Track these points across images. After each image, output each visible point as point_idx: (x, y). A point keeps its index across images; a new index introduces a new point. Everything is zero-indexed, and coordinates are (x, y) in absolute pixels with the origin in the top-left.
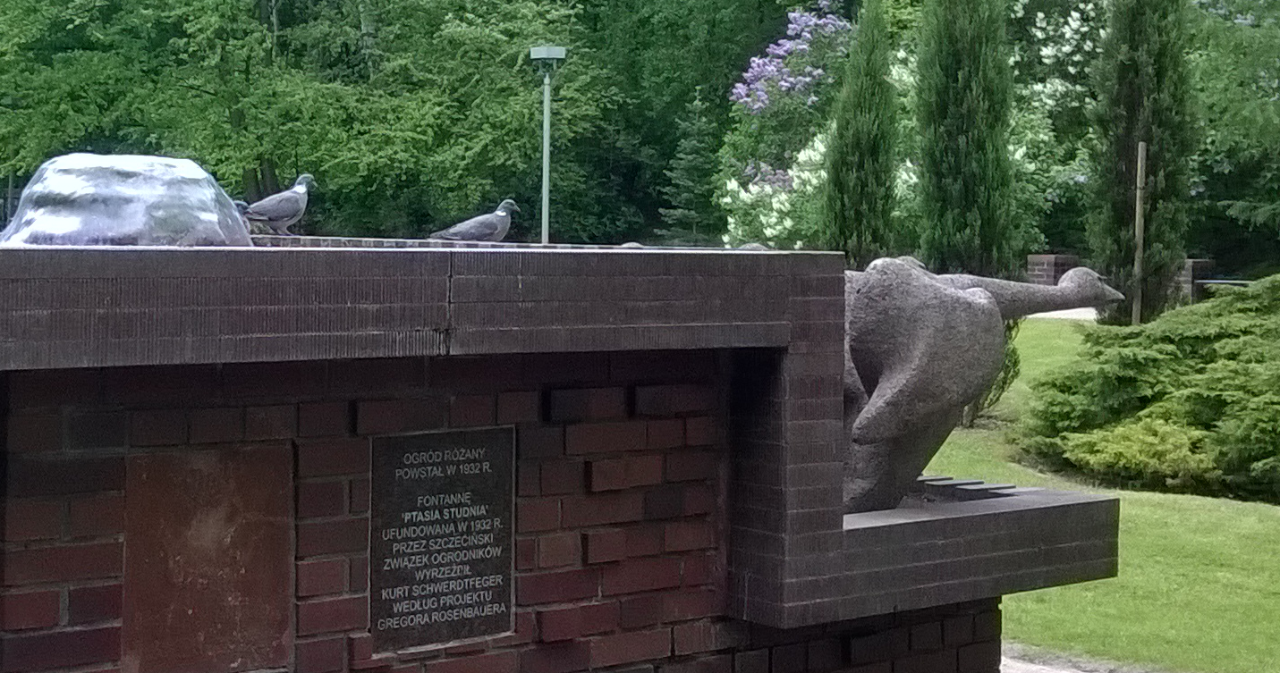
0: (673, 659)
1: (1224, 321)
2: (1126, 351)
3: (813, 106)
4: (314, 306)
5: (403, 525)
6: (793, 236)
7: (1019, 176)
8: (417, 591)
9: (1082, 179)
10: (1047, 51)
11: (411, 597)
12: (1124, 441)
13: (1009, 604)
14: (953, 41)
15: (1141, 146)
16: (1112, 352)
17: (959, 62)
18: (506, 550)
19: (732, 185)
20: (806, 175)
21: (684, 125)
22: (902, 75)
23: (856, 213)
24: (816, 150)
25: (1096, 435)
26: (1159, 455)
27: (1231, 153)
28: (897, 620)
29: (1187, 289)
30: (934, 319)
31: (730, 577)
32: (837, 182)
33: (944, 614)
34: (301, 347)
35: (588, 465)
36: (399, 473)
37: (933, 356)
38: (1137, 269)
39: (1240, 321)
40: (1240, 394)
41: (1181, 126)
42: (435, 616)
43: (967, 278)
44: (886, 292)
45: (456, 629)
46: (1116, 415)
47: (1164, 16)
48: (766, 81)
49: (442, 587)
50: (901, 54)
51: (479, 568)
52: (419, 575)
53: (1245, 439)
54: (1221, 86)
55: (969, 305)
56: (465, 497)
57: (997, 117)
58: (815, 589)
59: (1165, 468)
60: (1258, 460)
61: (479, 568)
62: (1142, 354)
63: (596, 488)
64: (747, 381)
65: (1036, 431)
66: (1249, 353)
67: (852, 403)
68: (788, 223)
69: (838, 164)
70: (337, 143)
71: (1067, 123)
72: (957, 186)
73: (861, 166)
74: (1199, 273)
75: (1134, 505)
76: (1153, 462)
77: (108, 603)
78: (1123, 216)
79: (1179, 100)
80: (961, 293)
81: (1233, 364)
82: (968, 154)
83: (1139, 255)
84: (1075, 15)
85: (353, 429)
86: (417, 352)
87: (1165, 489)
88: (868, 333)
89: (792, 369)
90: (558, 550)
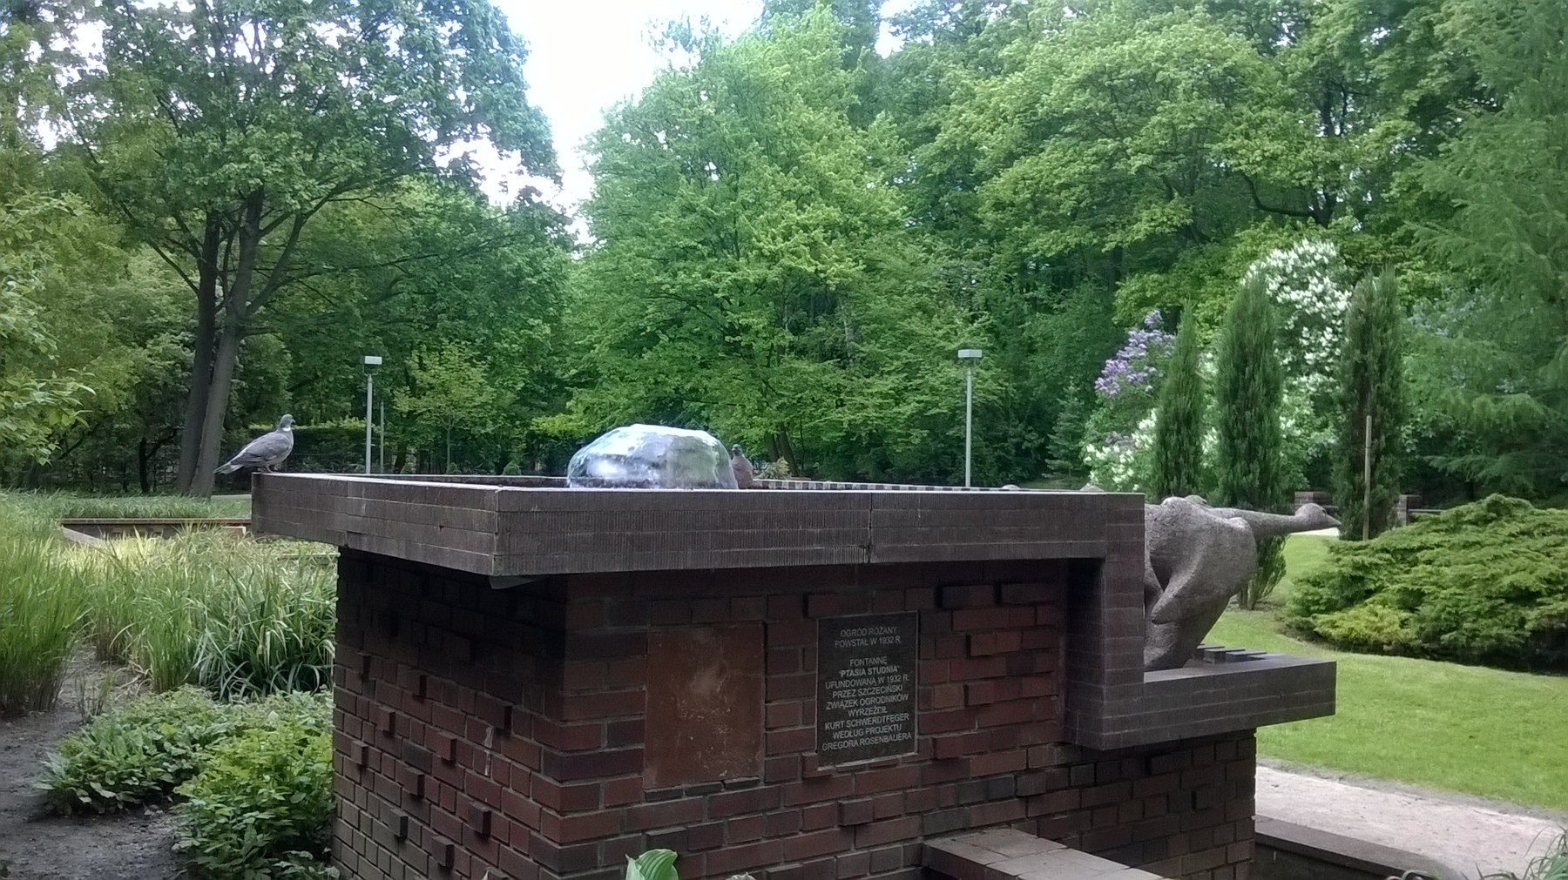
0: (1028, 771)
1: (1423, 538)
2: (1357, 559)
3: (1150, 392)
4: (776, 530)
5: (839, 679)
6: (1134, 480)
7: (1289, 439)
8: (849, 724)
9: (1332, 441)
10: (1309, 356)
11: (845, 728)
12: (1356, 620)
13: (1262, 732)
14: (1242, 347)
15: (1369, 419)
16: (1347, 559)
17: (1246, 361)
18: (911, 696)
19: (1091, 448)
20: (1144, 437)
21: (1063, 402)
22: (1209, 367)
23: (1175, 467)
24: (1150, 422)
25: (1336, 616)
26: (1379, 630)
27: (1434, 424)
28: (1181, 745)
29: (1401, 515)
30: (1206, 540)
31: (1067, 715)
32: (1163, 442)
33: (1217, 740)
34: (769, 557)
35: (968, 638)
36: (837, 643)
37: (1207, 563)
38: (1366, 502)
39: (1434, 538)
40: (1434, 588)
41: (1396, 406)
42: (863, 742)
43: (1232, 510)
44: (1175, 520)
45: (875, 750)
46: (1350, 602)
47: (1385, 330)
48: (1116, 377)
49: (867, 721)
50: (1209, 355)
51: (893, 708)
52: (851, 713)
53: (1437, 619)
54: (1425, 378)
55: (1231, 530)
56: (883, 661)
57: (1272, 398)
58: (1124, 723)
59: (1383, 638)
60: (1445, 632)
61: (893, 708)
62: (1367, 560)
63: (974, 652)
64: (1078, 581)
65: (1297, 613)
66: (1441, 560)
67: (1150, 596)
68: (1131, 472)
69: (1163, 432)
70: (829, 407)
71: (1322, 403)
72: (1244, 446)
73: (1179, 432)
74: (1411, 505)
75: (1349, 664)
76: (1374, 634)
77: (634, 732)
78: (1357, 466)
79: (1395, 387)
80: (1226, 521)
81: (1429, 568)
82: (1251, 424)
83: (1367, 492)
84: (1329, 330)
85: (805, 612)
86: (848, 561)
87: (1383, 653)
88: (1162, 548)
89: (1108, 573)
90: (948, 696)
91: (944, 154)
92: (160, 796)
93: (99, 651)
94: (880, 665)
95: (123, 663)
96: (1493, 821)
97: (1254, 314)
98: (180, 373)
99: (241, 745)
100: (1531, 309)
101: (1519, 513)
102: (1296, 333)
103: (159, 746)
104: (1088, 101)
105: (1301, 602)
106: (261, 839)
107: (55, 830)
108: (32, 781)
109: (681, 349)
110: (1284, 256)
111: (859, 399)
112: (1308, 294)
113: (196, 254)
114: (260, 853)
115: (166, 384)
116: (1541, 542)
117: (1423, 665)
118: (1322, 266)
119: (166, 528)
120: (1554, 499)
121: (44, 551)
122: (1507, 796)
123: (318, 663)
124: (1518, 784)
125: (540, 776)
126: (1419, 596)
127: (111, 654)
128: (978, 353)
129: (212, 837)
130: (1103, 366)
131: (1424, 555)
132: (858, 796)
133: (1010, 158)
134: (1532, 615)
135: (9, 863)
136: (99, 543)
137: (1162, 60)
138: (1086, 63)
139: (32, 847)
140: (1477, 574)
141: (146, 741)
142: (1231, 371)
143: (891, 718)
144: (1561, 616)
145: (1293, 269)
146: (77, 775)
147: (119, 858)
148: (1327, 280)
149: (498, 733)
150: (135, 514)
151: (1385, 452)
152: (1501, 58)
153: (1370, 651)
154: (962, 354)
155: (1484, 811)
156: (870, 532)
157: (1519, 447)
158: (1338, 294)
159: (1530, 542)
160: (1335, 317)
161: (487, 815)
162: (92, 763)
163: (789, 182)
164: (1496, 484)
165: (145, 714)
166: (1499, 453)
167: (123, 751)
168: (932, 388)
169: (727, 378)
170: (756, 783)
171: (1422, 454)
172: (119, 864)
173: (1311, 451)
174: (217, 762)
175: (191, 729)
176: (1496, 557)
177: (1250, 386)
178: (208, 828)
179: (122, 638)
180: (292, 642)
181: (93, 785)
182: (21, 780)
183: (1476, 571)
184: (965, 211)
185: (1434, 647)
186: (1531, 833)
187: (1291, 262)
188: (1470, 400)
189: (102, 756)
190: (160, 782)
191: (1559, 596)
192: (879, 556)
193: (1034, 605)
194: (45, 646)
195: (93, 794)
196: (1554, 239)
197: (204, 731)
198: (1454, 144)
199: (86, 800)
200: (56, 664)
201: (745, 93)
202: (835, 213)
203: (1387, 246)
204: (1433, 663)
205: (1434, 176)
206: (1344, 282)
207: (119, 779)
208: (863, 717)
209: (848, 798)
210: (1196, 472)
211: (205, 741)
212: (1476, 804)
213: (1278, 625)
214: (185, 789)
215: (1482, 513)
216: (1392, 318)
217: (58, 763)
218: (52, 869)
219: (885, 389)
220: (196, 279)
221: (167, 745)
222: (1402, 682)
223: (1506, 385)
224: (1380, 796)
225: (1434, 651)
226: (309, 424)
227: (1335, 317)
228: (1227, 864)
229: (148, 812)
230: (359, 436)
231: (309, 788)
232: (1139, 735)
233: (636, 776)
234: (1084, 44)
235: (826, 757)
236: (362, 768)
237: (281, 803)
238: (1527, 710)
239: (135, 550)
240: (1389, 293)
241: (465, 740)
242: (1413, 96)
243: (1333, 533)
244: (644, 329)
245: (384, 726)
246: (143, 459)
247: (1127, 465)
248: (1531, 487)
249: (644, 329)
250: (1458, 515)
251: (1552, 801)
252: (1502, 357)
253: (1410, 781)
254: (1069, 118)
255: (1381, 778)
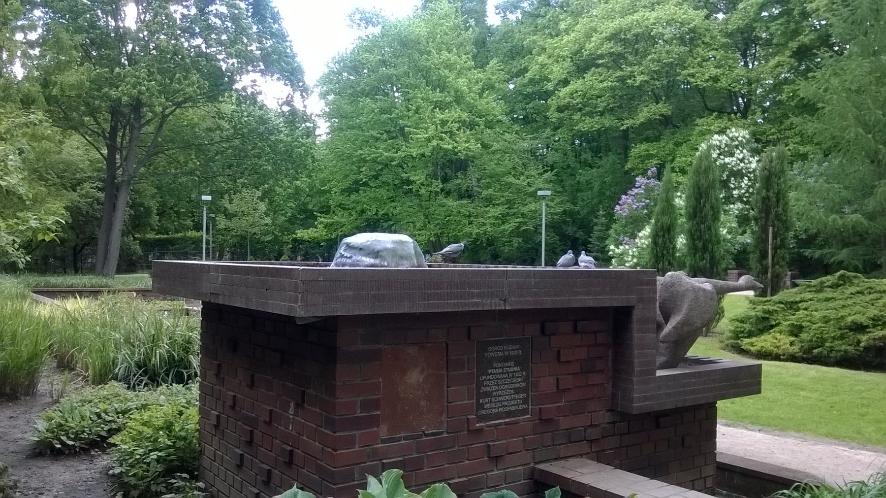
0: (591, 426)
1: (802, 296)
2: (765, 307)
3: (646, 214)
4: (454, 290)
5: (488, 375)
6: (636, 265)
7: (724, 240)
10: (735, 192)
12: (765, 342)
13: (720, 404)
14: (699, 188)
15: (771, 229)
17: (701, 196)
19: (612, 247)
20: (643, 241)
21: (595, 220)
22: (680, 201)
23: (662, 255)
24: (647, 231)
25: (754, 339)
26: (778, 347)
27: (806, 231)
28: (677, 411)
29: (789, 283)
30: (691, 295)
32: (655, 243)
33: (695, 408)
35: (559, 351)
37: (691, 309)
38: (769, 275)
39: (808, 296)
42: (501, 409)
44: (673, 285)
45: (509, 414)
46: (761, 332)
47: (779, 179)
48: (627, 205)
49: (502, 398)
50: (679, 194)
51: (517, 391)
52: (494, 394)
53: (811, 341)
55: (704, 290)
56: (512, 364)
57: (716, 218)
59: (780, 352)
61: (517, 391)
62: (771, 308)
63: (562, 359)
64: (618, 320)
65: (731, 338)
66: (813, 308)
67: (659, 327)
68: (635, 260)
69: (655, 236)
71: (743, 220)
73: (664, 236)
74: (793, 277)
75: (767, 366)
76: (776, 350)
77: (376, 404)
78: (764, 255)
79: (785, 211)
81: (806, 312)
83: (770, 270)
85: (469, 337)
87: (780, 360)
89: (636, 314)
90: (547, 384)
91: (531, 81)
92: (99, 443)
93: (58, 363)
94: (510, 367)
95: (73, 369)
96: (846, 453)
97: (705, 170)
98: (96, 207)
99: (146, 415)
100: (862, 169)
101: (856, 281)
102: (728, 180)
103: (99, 416)
104: (612, 48)
105: (734, 332)
106: (160, 468)
107: (41, 463)
108: (26, 436)
109: (378, 191)
110: (720, 138)
111: (481, 220)
112: (734, 159)
113: (105, 137)
114: (159, 476)
115: (87, 212)
116: (868, 298)
117: (803, 367)
118: (741, 144)
119: (94, 293)
120: (874, 273)
121: (26, 307)
122: (853, 439)
123: (186, 368)
124: (859, 433)
125: (323, 430)
126: (800, 328)
127: (65, 364)
128: (549, 193)
129: (132, 466)
130: (620, 199)
131: (804, 305)
132: (498, 440)
133: (565, 82)
134: (864, 338)
135: (18, 481)
136: (56, 302)
137: (654, 24)
138: (612, 26)
139: (29, 473)
140: (833, 316)
141: (91, 413)
142: (693, 202)
143: (516, 396)
144: (880, 339)
145: (726, 144)
146: (53, 432)
147: (78, 479)
148: (745, 151)
149: (297, 405)
150: (72, 286)
151: (780, 247)
152: (844, 25)
153: (773, 359)
154: (540, 193)
155: (841, 448)
156: (506, 292)
157: (854, 244)
158: (751, 159)
159: (863, 297)
160: (750, 173)
161: (291, 452)
162: (61, 425)
163: (437, 96)
164: (840, 265)
165: (90, 398)
166: (843, 248)
167: (78, 419)
168: (523, 214)
169: (401, 207)
170: (441, 433)
171: (800, 248)
172: (78, 482)
173: (737, 247)
174: (133, 425)
175: (116, 406)
176: (844, 306)
177: (703, 212)
178: (130, 461)
179: (72, 355)
180: (171, 357)
181: (62, 438)
182: (20, 435)
183: (833, 314)
184: (541, 112)
185: (808, 357)
186: (867, 460)
187: (724, 142)
188: (827, 217)
189: (67, 421)
190: (100, 436)
191: (879, 328)
192: (511, 305)
193: (595, 333)
194: (30, 359)
195: (62, 443)
196: (875, 126)
197: (124, 407)
198: (818, 74)
199: (58, 446)
200: (36, 370)
201: (405, 44)
202: (465, 116)
203: (779, 131)
204: (809, 366)
205: (806, 89)
206: (755, 152)
207: (77, 434)
208: (501, 396)
209: (493, 441)
210: (674, 259)
211: (124, 412)
212: (836, 444)
213: (721, 345)
214: (116, 439)
215: (835, 281)
216: (783, 172)
217: (42, 425)
218: (41, 485)
219: (496, 214)
220: (105, 151)
221: (103, 415)
222: (792, 376)
223: (847, 210)
224: (782, 440)
225: (809, 359)
226: (168, 234)
227: (750, 173)
228: (701, 478)
229: (93, 453)
230: (198, 242)
231: (185, 439)
232: (656, 406)
233: (375, 429)
234: (609, 16)
235: (481, 418)
236: (217, 427)
237: (169, 447)
238: (863, 392)
239: (74, 305)
240: (781, 157)
241: (278, 410)
242: (794, 45)
243: (751, 293)
244: (362, 180)
245: (229, 403)
246: (75, 254)
247: (633, 256)
248: (861, 267)
249: (362, 180)
250: (822, 283)
251: (878, 442)
252: (844, 193)
253: (799, 431)
254: (601, 56)
255: (782, 430)
